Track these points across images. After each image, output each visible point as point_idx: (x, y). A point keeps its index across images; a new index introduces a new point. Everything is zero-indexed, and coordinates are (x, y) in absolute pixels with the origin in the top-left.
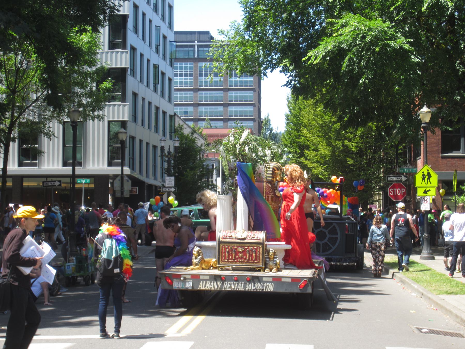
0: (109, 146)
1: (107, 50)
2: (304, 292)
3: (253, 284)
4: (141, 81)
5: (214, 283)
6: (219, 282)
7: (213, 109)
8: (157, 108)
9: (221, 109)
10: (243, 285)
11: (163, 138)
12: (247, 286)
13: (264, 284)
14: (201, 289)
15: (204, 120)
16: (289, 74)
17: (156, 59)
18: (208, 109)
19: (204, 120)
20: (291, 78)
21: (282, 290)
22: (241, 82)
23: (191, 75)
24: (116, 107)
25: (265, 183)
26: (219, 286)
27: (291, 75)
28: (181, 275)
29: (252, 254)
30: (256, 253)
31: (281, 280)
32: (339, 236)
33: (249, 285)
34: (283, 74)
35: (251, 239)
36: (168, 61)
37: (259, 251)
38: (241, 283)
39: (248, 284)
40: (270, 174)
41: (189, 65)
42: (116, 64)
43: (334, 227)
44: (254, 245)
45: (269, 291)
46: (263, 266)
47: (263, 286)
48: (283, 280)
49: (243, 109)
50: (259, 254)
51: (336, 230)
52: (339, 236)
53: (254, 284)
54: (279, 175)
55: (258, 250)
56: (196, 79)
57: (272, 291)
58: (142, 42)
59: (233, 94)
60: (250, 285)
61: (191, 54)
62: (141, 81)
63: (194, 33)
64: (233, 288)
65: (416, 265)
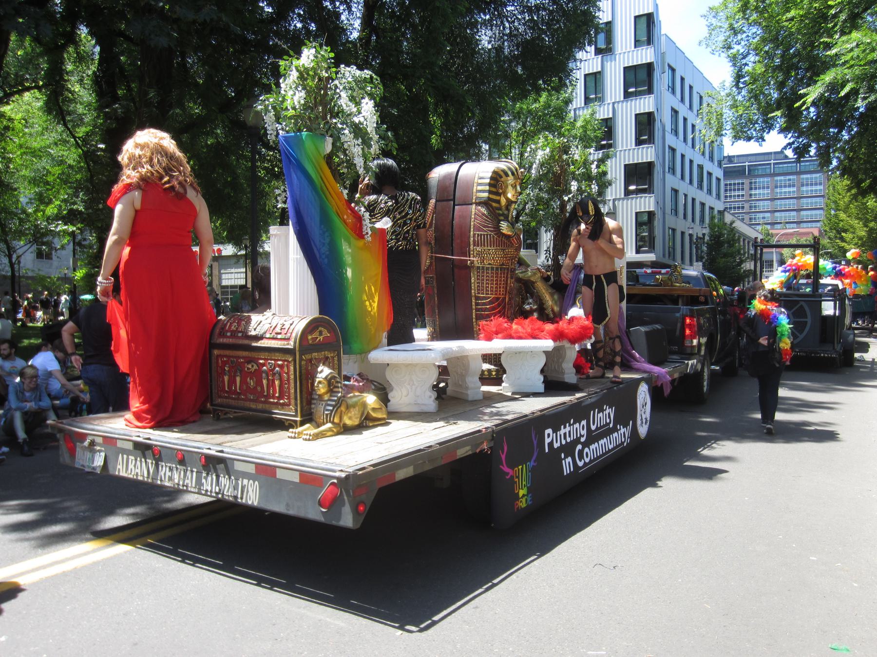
0: (637, 235)
1: (634, 147)
2: (334, 523)
3: (214, 477)
4: (683, 178)
5: (141, 461)
6: (149, 461)
7: (787, 214)
8: (703, 205)
9: (794, 213)
10: (194, 474)
11: (692, 225)
12: (204, 481)
13: (237, 479)
14: (121, 474)
15: (780, 223)
16: (790, 135)
17: (698, 160)
18: (783, 214)
19: (780, 223)
20: (792, 140)
21: (278, 507)
22: (812, 191)
23: (768, 188)
24: (643, 199)
25: (474, 206)
26: (151, 471)
27: (792, 136)
28: (86, 435)
29: (273, 381)
30: (281, 380)
31: (274, 474)
32: (809, 320)
33: (206, 478)
34: (782, 136)
35: (273, 338)
36: (716, 163)
37: (288, 373)
38: (192, 471)
39: (204, 475)
40: (485, 184)
41: (766, 179)
42: (642, 159)
43: (802, 307)
44: (278, 356)
45: (250, 502)
46: (296, 416)
47: (235, 488)
48: (280, 474)
49: (814, 212)
50: (288, 380)
51: (805, 311)
52: (809, 320)
53: (218, 477)
54: (510, 188)
55: (286, 370)
56: (772, 190)
57: (256, 504)
58: (684, 144)
59: (805, 200)
60: (209, 478)
61: (768, 171)
62: (683, 178)
63: (771, 153)
64: (176, 481)
65: (723, 475)
